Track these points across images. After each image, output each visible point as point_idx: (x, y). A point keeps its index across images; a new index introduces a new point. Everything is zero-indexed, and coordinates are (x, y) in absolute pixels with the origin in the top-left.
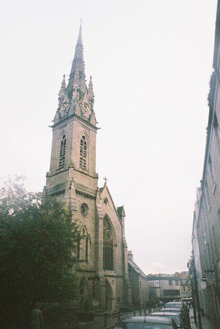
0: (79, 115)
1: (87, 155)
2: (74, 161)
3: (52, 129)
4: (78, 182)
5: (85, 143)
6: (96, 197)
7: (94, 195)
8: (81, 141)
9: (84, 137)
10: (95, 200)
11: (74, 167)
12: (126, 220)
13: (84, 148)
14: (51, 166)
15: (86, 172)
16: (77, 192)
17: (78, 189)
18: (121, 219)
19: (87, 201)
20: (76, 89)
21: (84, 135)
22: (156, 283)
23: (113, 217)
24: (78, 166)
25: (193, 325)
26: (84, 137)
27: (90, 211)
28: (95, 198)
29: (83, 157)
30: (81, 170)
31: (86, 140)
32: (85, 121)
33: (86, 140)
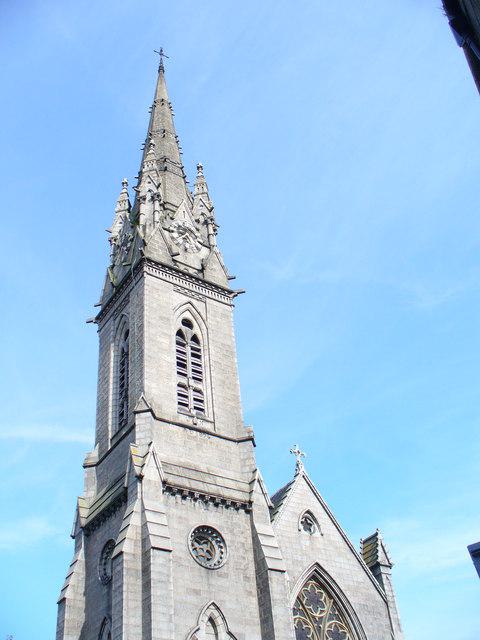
0: (166, 260)
1: (206, 375)
2: (154, 391)
3: (96, 327)
4: (174, 459)
5: (195, 338)
6: (250, 503)
7: (244, 497)
8: (180, 333)
9: (187, 323)
10: (248, 512)
11: (150, 410)
12: (394, 578)
13: (193, 355)
14: (97, 432)
15: (208, 427)
16: (169, 488)
17: (171, 480)
18: (378, 576)
19: (213, 518)
20: (149, 197)
21: (187, 315)
22: (137, 376)
23: (349, 575)
24: (169, 407)
25: (469, 3)
26: (187, 323)
27: (236, 554)
28: (247, 507)
29: (192, 382)
30: (183, 419)
31: (196, 330)
32: (191, 277)
33: (196, 330)
